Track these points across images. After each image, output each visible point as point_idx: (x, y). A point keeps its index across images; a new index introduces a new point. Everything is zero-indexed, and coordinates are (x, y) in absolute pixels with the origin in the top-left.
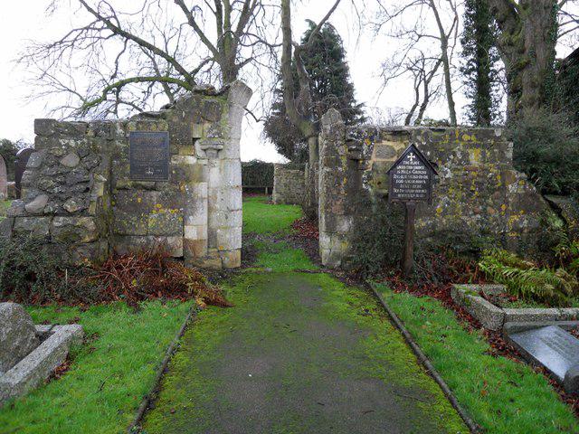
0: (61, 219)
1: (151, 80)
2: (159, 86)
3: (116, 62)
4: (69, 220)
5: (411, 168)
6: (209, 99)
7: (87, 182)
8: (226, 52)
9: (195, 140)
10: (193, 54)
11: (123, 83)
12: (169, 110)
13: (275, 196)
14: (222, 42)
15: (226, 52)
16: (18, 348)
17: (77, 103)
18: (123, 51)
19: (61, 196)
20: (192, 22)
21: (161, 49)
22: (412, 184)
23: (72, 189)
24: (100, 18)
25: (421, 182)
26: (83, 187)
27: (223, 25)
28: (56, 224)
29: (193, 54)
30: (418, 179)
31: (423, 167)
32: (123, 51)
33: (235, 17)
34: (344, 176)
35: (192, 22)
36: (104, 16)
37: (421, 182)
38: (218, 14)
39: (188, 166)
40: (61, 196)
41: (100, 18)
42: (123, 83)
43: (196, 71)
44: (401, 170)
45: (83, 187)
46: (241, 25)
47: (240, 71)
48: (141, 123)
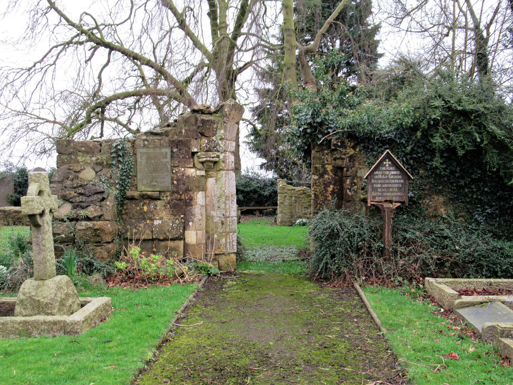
0: (84, 223)
1: (138, 94)
2: (147, 100)
3: (100, 77)
4: (90, 224)
5: (388, 172)
6: (205, 117)
7: (102, 192)
8: (222, 62)
9: (193, 154)
10: (185, 61)
11: (108, 101)
12: (170, 128)
13: (279, 217)
14: (218, 43)
15: (222, 62)
16: (71, 305)
17: (152, 127)
18: (107, 64)
19: (82, 204)
20: (182, 25)
21: (147, 56)
22: (388, 188)
23: (91, 199)
24: (83, 32)
25: (396, 186)
26: (100, 196)
27: (217, 27)
28: (79, 227)
29: (185, 61)
30: (395, 183)
31: (398, 173)
32: (107, 64)
33: (231, 16)
34: (330, 183)
35: (182, 25)
36: (85, 28)
37: (396, 186)
38: (212, 15)
39: (188, 177)
40: (82, 204)
41: (83, 32)
42: (108, 101)
43: (188, 81)
44: (377, 175)
45: (100, 196)
46: (239, 25)
47: (239, 77)
48: (147, 140)
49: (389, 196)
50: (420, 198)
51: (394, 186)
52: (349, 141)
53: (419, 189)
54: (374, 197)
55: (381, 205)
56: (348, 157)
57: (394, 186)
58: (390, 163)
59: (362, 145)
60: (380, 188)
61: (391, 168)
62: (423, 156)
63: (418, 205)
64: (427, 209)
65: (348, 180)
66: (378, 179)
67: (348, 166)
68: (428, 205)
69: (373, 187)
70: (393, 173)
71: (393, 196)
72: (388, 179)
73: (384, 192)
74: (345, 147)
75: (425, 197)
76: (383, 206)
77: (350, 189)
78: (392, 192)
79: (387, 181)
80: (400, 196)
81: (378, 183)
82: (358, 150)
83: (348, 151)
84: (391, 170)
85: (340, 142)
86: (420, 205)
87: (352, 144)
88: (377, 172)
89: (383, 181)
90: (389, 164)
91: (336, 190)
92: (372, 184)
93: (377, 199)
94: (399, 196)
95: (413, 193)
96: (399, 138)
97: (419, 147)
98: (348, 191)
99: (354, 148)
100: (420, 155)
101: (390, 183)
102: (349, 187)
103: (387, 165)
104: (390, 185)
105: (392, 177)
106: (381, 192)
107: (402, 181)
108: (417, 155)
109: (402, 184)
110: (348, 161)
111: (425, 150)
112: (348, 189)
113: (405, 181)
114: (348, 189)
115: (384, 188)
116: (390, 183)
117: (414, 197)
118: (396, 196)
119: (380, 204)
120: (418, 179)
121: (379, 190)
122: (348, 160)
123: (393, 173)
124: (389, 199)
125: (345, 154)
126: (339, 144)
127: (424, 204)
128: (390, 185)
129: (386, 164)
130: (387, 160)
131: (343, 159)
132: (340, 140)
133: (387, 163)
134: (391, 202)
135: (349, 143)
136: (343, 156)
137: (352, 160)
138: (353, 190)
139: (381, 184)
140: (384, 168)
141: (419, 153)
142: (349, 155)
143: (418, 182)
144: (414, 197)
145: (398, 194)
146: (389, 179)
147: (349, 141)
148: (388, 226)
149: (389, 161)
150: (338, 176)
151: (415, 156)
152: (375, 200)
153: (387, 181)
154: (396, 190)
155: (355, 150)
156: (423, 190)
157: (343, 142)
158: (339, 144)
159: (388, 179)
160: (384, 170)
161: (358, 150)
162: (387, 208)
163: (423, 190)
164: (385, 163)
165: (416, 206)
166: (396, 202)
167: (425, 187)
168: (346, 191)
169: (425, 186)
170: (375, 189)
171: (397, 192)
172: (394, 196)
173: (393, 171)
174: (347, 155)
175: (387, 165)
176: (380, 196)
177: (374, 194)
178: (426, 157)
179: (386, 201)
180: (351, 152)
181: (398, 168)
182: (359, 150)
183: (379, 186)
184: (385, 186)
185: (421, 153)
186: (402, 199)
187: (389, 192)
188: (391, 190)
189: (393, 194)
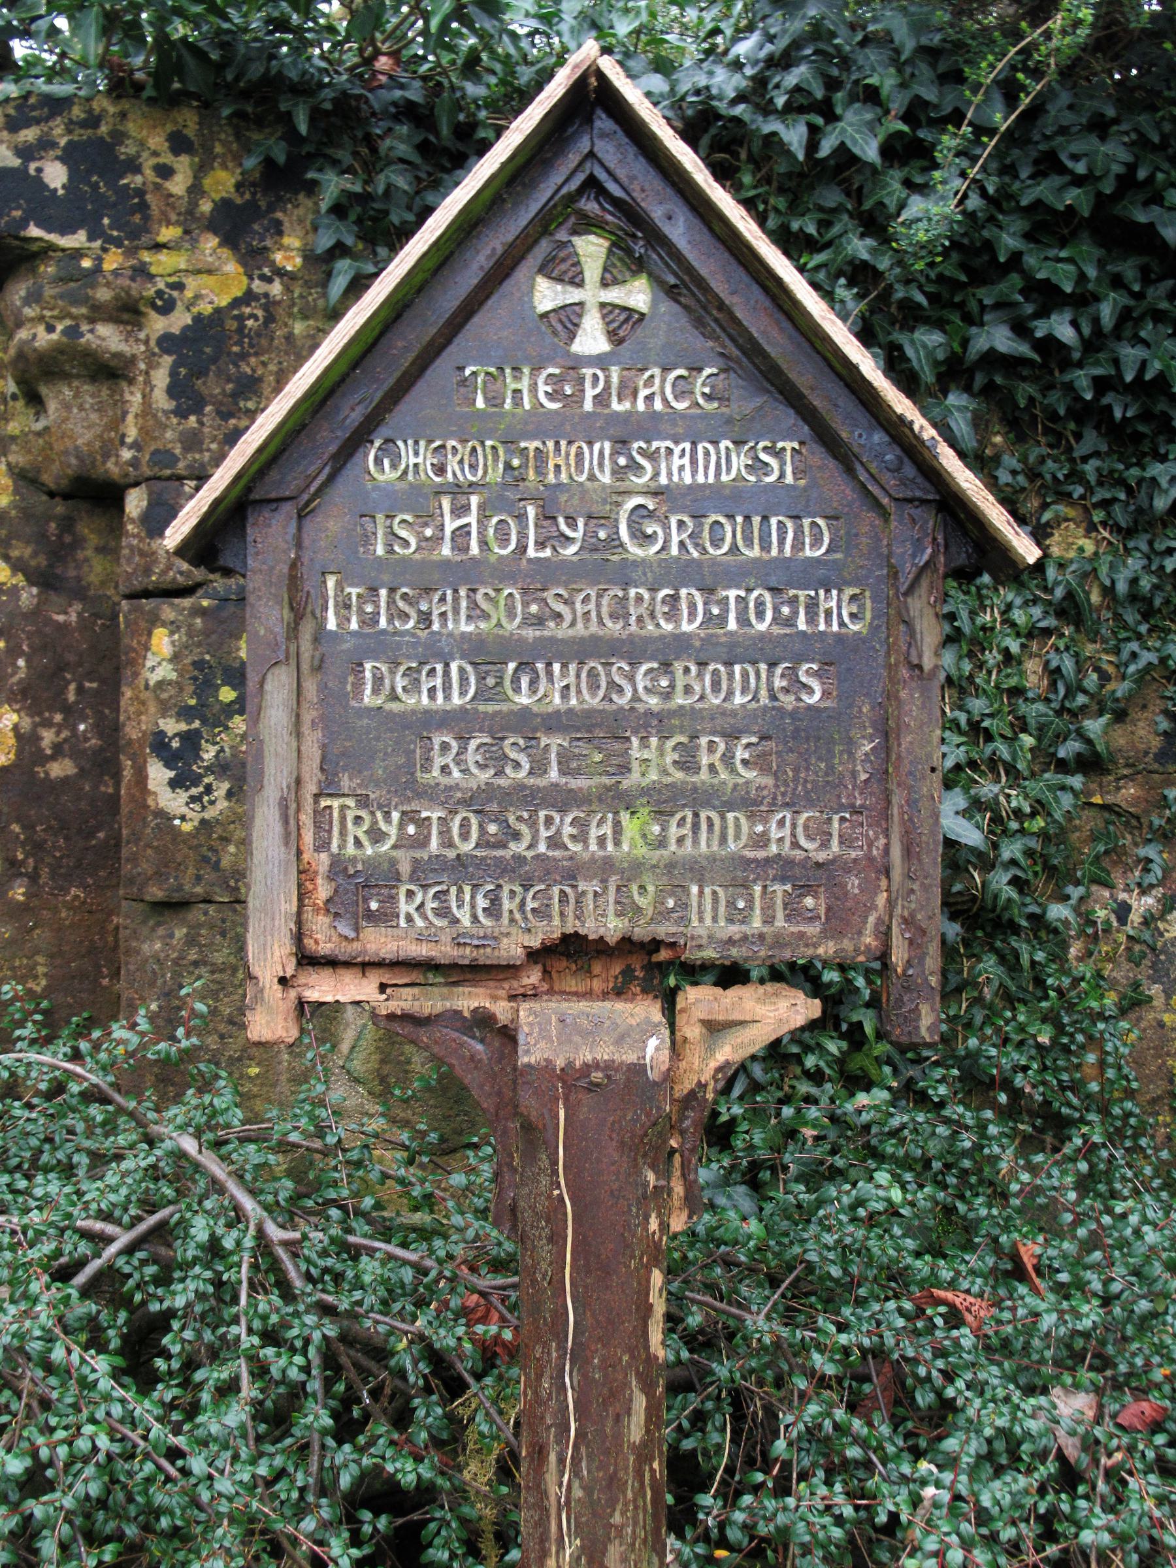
5: (596, 462)
22: (609, 729)
25: (743, 690)
31: (782, 462)
37: (743, 690)
44: (420, 502)
49: (631, 862)
50: (1051, 868)
51: (693, 688)
52: (179, 144)
53: (1047, 759)
54: (362, 891)
55: (483, 1021)
56: (167, 342)
57: (693, 688)
58: (637, 294)
59: (333, 185)
60: (460, 723)
61: (658, 391)
62: (1094, 343)
63: (1028, 953)
64: (1134, 1003)
65: (162, 642)
66: (428, 578)
67: (163, 457)
68: (1147, 948)
69: (336, 716)
70: (680, 466)
71: (680, 874)
72: (604, 567)
73: (530, 798)
74: (130, 221)
75: (1116, 853)
76: (508, 1035)
77: (182, 759)
78: (664, 802)
79: (582, 614)
80: (804, 876)
81: (433, 652)
82: (288, 255)
83: (163, 263)
84: (650, 426)
85: (68, 157)
86: (1059, 957)
87: (223, 182)
88: (415, 457)
89: (506, 616)
90: (622, 323)
91: (59, 769)
92: (333, 665)
93: (414, 925)
94: (784, 868)
95: (976, 805)
96: (799, 104)
97: (1048, 226)
98: (158, 774)
99: (240, 227)
100: (1062, 327)
101: (632, 651)
102: (171, 726)
103: (591, 339)
104: (639, 687)
105: (674, 536)
106: (478, 802)
107: (839, 613)
108: (1021, 329)
109: (835, 655)
110: (161, 400)
111: (1129, 269)
112: (160, 745)
113: (895, 617)
114: (160, 745)
115: (528, 724)
116: (632, 651)
117: (987, 862)
118: (741, 873)
119: (469, 1000)
120: (1033, 633)
121: (458, 766)
122: (161, 378)
123: (680, 466)
124: (612, 927)
125: (128, 313)
126: (55, 175)
127: (1091, 931)
128: (639, 687)
129: (568, 319)
130: (591, 250)
131: (109, 372)
132: (58, 131)
133: (591, 294)
134: (655, 968)
135: (183, 166)
136: (108, 338)
137: (213, 387)
138: (221, 768)
139: (485, 655)
140: (533, 391)
141: (1048, 297)
142: (179, 320)
143: (1032, 674)
144: (987, 862)
145: (781, 833)
146: (626, 573)
147: (179, 144)
148: (601, 1403)
149: (626, 260)
150: (79, 592)
151: (999, 338)
152: (379, 942)
153: (582, 614)
154: (732, 765)
155: (254, 260)
156: (1091, 763)
157: (96, 158)
158: (55, 175)
159: (604, 567)
160: (541, 424)
161: (288, 255)
162: (575, 1081)
163: (1091, 763)
164: (547, 295)
165: (1011, 962)
166: (731, 975)
167: (1120, 738)
168: (141, 778)
169: (1120, 716)
170: (368, 755)
171: (751, 804)
172: (698, 870)
173: (694, 430)
174: (158, 325)
175: (591, 339)
176: (461, 869)
177: (362, 835)
178: (1131, 354)
179: (569, 953)
180: (209, 278)
181: (778, 377)
182: (309, 257)
183: (450, 689)
184: (557, 690)
185: (1082, 300)
186: (838, 920)
187: (618, 800)
188: (651, 762)
189: (684, 841)
